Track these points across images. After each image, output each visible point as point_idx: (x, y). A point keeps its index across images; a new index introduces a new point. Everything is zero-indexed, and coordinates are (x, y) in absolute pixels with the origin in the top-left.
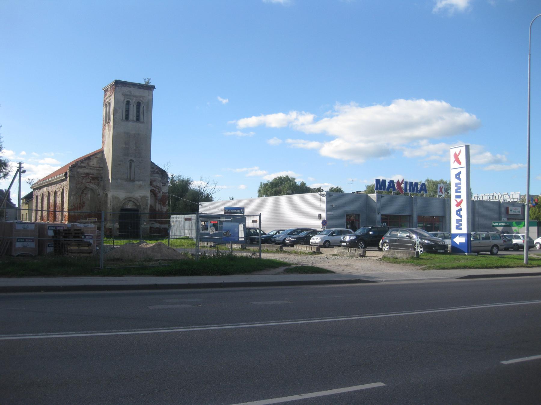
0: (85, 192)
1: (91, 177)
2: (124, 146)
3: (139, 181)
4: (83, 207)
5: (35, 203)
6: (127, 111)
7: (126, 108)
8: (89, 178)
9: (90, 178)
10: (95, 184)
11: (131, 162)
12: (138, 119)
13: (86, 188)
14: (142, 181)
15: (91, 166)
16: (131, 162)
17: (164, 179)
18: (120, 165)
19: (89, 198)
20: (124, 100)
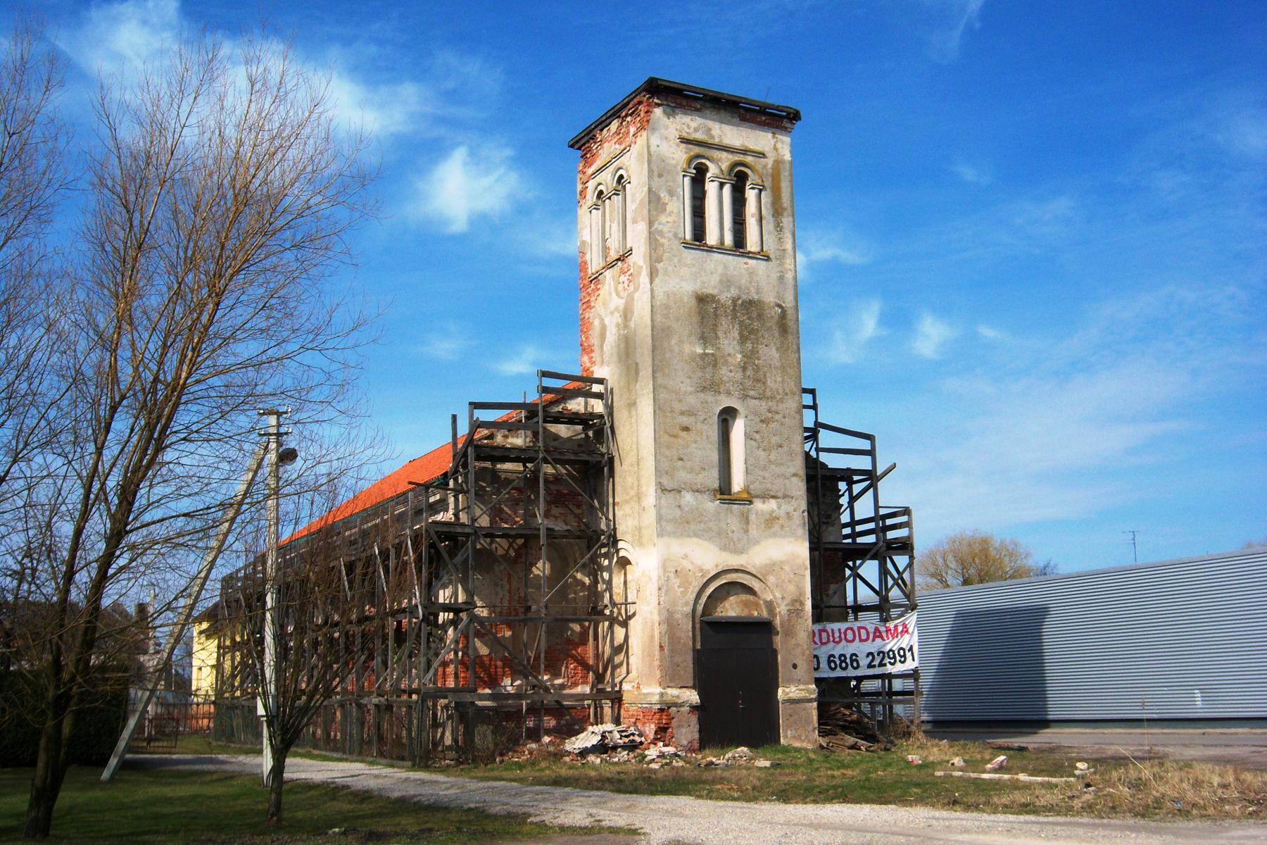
14: (774, 497)
18: (686, 429)
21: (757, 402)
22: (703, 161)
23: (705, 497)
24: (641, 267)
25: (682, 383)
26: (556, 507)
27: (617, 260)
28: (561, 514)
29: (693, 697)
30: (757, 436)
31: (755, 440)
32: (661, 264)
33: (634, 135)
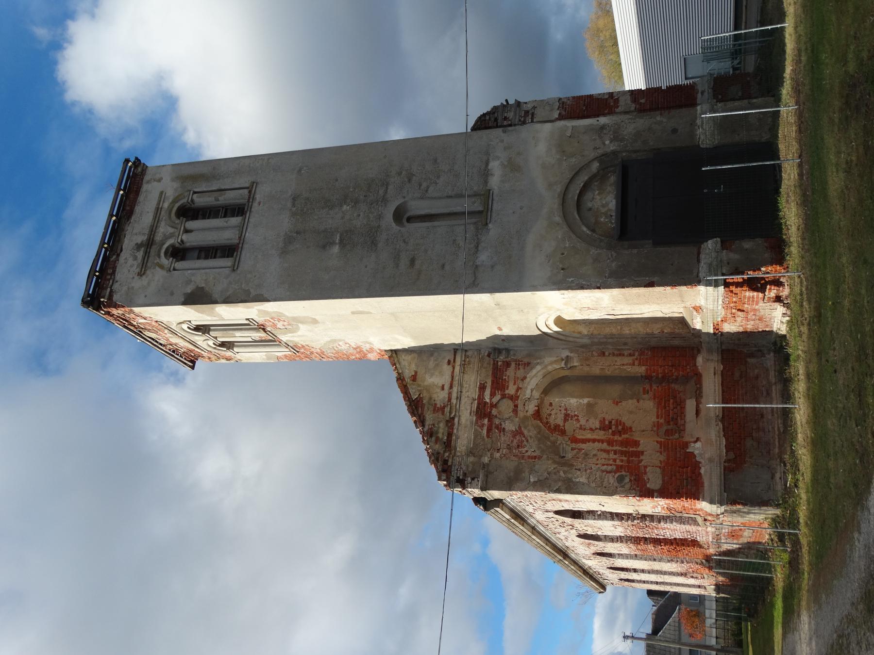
0: (557, 419)
1: (493, 395)
2: (336, 249)
3: (486, 174)
4: (626, 429)
5: (666, 577)
6: (208, 252)
7: (198, 258)
8: (493, 406)
9: (498, 397)
10: (525, 378)
11: (406, 217)
12: (239, 210)
13: (537, 414)
14: (487, 164)
15: (447, 396)
16: (406, 217)
17: (505, 118)
18: (412, 261)
19: (586, 401)
20: (162, 267)
21: (391, 187)
22: (165, 246)
23: (483, 239)
24: (259, 311)
25: (366, 267)
26: (507, 389)
27: (265, 332)
28: (515, 384)
29: (711, 245)
30: (424, 185)
31: (428, 187)
32: (252, 291)
33: (145, 319)
